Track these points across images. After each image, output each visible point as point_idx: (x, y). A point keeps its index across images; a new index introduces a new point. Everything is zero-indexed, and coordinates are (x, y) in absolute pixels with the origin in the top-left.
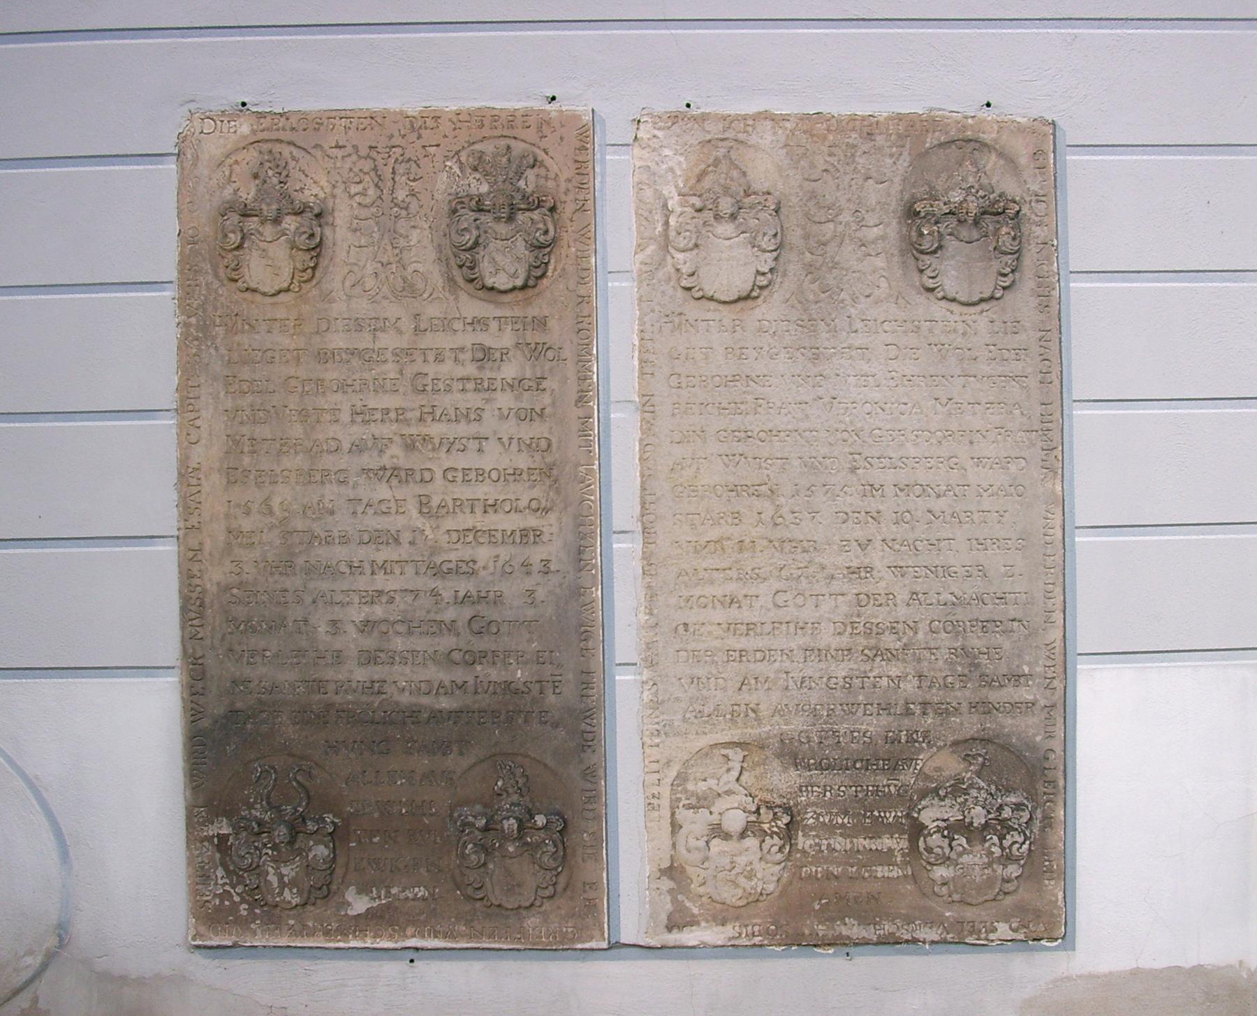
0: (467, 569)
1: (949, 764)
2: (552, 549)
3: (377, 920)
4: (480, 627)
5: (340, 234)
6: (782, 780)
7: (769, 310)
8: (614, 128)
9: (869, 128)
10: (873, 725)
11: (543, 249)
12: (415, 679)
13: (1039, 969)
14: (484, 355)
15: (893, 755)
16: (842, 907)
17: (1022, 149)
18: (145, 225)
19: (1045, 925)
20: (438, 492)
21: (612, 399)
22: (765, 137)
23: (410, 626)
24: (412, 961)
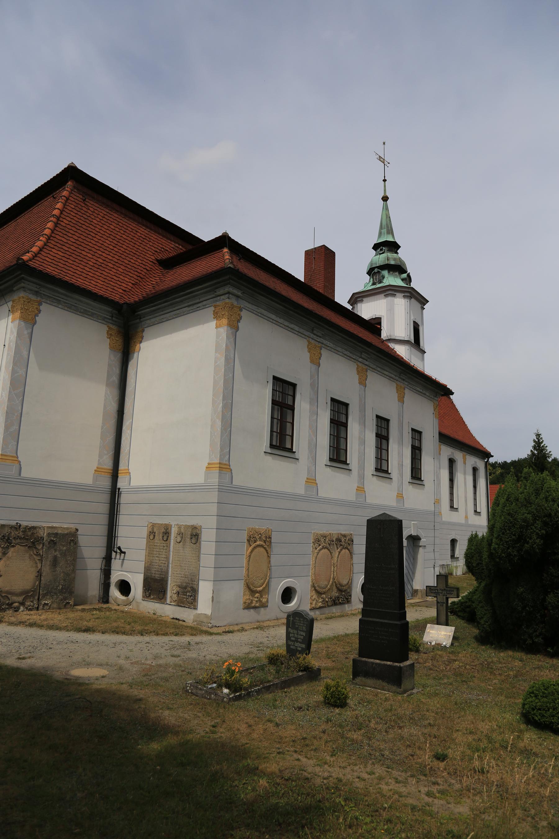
0: (161, 566)
1: (189, 589)
2: (166, 565)
3: (153, 599)
4: (162, 572)
5: (156, 534)
6: (178, 589)
7: (181, 543)
8: (173, 526)
9: (189, 526)
10: (185, 584)
11: (168, 537)
12: (157, 576)
13: (195, 612)
14: (164, 546)
15: (185, 588)
16: (183, 603)
17: (199, 528)
18: (144, 532)
19: (195, 608)
20: (161, 559)
21: (463, 522)
22: (379, 326)
23: (158, 571)
24: (154, 614)
